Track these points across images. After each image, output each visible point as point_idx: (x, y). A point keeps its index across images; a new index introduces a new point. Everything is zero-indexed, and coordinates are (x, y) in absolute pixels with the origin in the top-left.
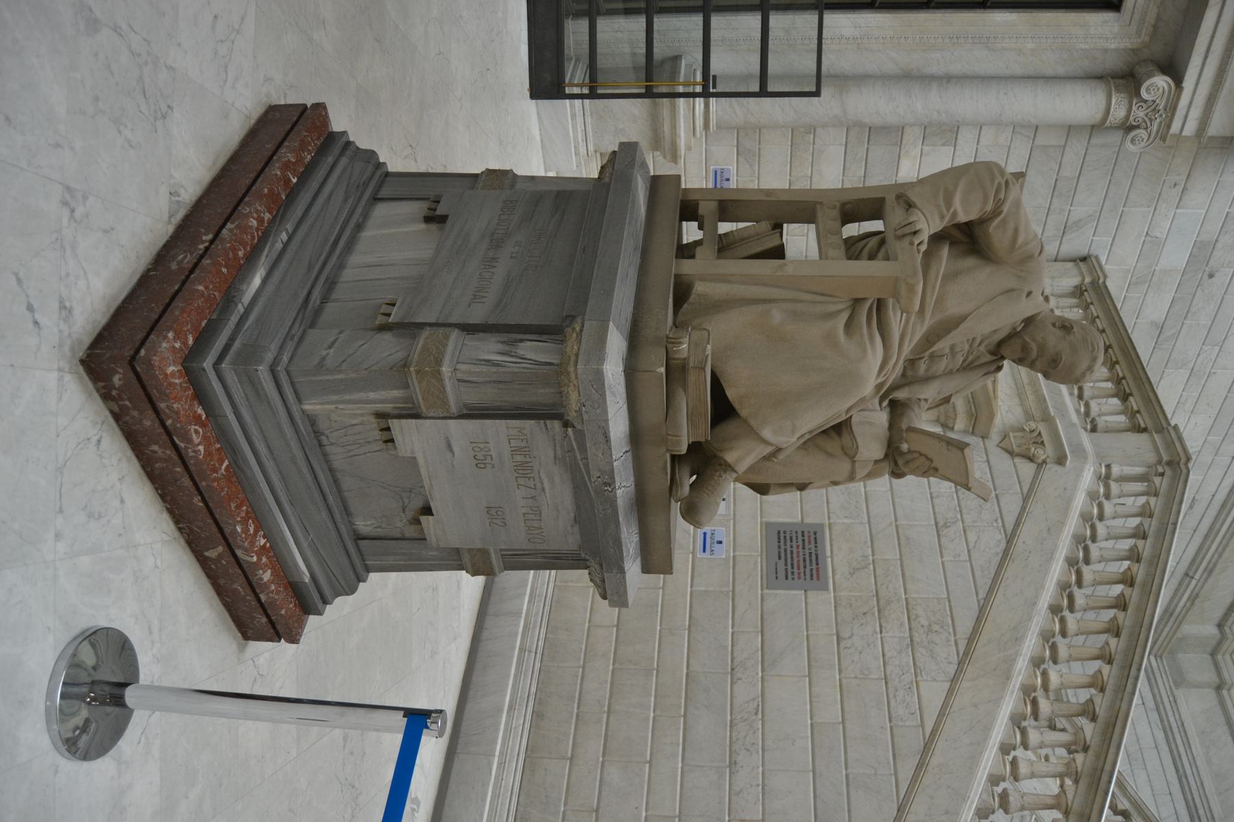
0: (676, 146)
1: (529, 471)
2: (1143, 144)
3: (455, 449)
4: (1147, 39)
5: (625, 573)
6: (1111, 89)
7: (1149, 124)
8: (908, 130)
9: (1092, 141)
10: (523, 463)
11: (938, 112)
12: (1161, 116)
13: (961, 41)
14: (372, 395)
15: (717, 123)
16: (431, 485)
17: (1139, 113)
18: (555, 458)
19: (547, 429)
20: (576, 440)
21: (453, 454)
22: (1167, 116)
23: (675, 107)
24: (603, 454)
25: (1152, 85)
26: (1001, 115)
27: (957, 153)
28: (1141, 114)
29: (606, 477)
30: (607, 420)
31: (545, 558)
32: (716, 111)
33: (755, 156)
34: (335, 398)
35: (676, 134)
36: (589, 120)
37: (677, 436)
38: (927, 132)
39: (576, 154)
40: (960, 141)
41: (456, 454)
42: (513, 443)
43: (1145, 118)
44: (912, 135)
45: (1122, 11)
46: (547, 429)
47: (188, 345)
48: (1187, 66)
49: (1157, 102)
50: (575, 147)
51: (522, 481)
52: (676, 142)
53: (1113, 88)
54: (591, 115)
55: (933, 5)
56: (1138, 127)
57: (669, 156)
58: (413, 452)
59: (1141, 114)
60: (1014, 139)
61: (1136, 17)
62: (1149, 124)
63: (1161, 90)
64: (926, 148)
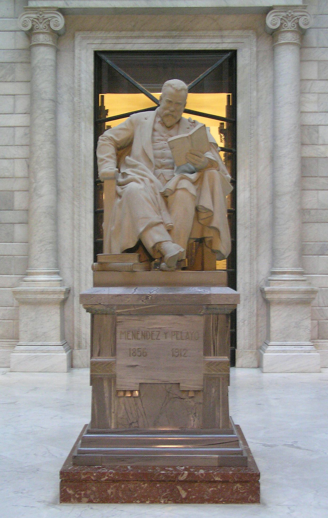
0: (305, 292)
1: (148, 333)
2: (308, 18)
3: (134, 363)
4: (251, 31)
5: (211, 294)
6: (277, 45)
7: (296, 18)
8: (304, 155)
9: (315, 45)
10: (142, 335)
11: (289, 139)
12: (290, 13)
13: (252, 132)
14: (107, 395)
15: (294, 267)
16: (158, 379)
17: (289, 25)
18: (139, 320)
19: (121, 322)
20: (123, 309)
21: (137, 365)
22: (290, 9)
23: (280, 291)
24: (128, 298)
25: (271, 23)
26: (291, 103)
27: (323, 123)
28: (289, 24)
29: (142, 298)
30: (109, 295)
31: (216, 335)
32: (287, 267)
33: (324, 245)
34: (108, 412)
35: (298, 291)
36: (289, 343)
37: (125, 266)
38: (310, 143)
39: (309, 353)
40: (315, 123)
41: (137, 364)
42: (130, 337)
43: (291, 22)
44: (309, 152)
45: (236, 49)
46: (121, 322)
47: (101, 478)
48: (263, 7)
49: (281, 17)
50: (305, 352)
51: (155, 337)
52: (302, 291)
53: (277, 43)
54: (285, 341)
55: (234, 150)
56: (298, 24)
57: (313, 296)
58: (136, 384)
59: (289, 24)
60: (314, 92)
61: (239, 40)
62: (296, 18)
63: (274, 17)
64: (321, 142)
